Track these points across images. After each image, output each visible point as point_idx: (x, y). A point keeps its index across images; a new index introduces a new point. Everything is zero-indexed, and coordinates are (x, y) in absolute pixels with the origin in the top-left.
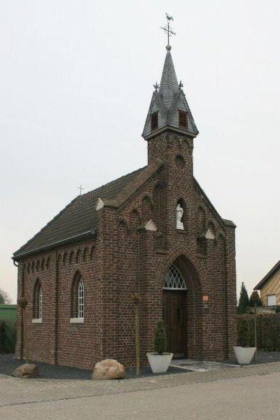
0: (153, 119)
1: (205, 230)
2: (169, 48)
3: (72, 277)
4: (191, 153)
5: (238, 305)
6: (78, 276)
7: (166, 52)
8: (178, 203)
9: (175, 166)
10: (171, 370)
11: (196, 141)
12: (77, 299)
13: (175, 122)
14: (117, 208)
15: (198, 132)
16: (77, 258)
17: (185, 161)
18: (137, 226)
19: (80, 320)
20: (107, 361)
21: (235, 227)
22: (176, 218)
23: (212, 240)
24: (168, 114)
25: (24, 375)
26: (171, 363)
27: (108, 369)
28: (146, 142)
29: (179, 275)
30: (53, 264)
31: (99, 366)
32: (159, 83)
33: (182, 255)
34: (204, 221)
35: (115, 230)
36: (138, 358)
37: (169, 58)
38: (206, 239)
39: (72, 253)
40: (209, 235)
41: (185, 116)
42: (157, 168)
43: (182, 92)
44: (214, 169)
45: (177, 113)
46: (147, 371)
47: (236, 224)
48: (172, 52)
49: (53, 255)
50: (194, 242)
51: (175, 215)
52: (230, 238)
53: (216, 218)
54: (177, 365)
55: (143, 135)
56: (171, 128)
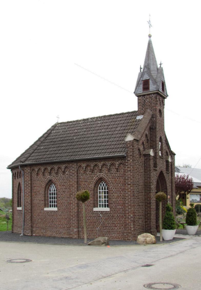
2: (150, 36)
5: (55, 209)
7: (148, 39)
15: (168, 96)
20: (145, 234)
21: (174, 154)
25: (103, 244)
27: (146, 239)
28: (137, 98)
31: (139, 237)
37: (150, 44)
45: (161, 82)
47: (175, 153)
48: (152, 39)
50: (165, 163)
53: (169, 149)
54: (177, 236)
55: (134, 93)
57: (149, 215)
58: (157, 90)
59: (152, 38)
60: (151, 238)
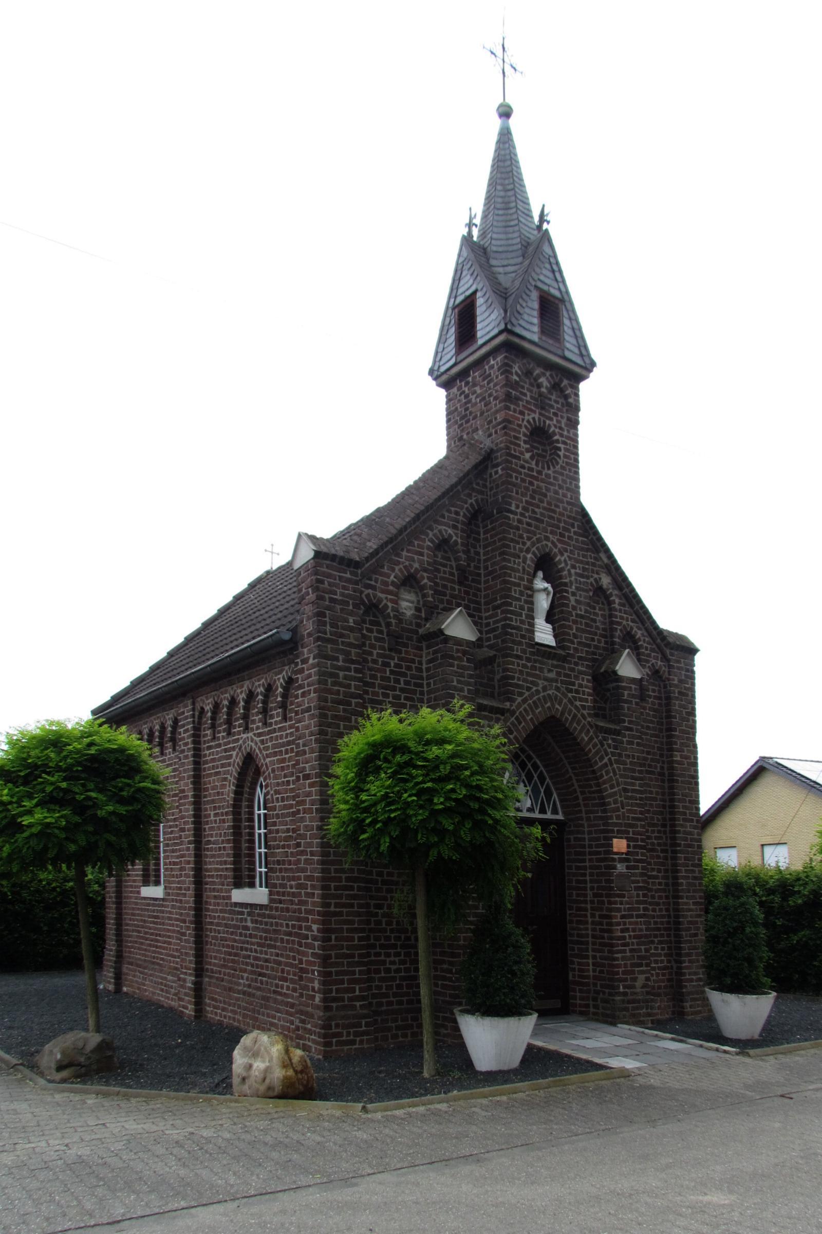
0: (463, 317)
1: (613, 653)
2: (505, 113)
3: (234, 770)
4: (574, 423)
6: (250, 770)
7: (496, 123)
8: (537, 569)
9: (528, 456)
10: (536, 1063)
11: (588, 391)
12: (252, 834)
13: (530, 327)
14: (356, 565)
16: (246, 717)
17: (550, 442)
18: (419, 625)
19: (259, 895)
21: (693, 651)
22: (531, 610)
23: (633, 680)
24: (503, 297)
26: (535, 1034)
28: (442, 393)
29: (542, 779)
30: (185, 735)
32: (479, 210)
33: (553, 717)
34: (609, 632)
35: (351, 629)
36: (426, 1016)
37: (505, 140)
38: (619, 679)
39: (233, 702)
40: (627, 668)
41: (554, 309)
42: (474, 458)
43: (546, 237)
44: (632, 481)
45: (535, 295)
46: (457, 1068)
49: (185, 710)
50: (585, 683)
51: (531, 603)
52: (681, 681)
53: (643, 623)
55: (431, 372)
56: (516, 340)
57: (330, 940)
58: (501, 332)
59: (512, 122)
60: (267, 1064)
